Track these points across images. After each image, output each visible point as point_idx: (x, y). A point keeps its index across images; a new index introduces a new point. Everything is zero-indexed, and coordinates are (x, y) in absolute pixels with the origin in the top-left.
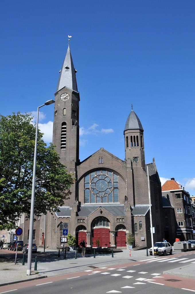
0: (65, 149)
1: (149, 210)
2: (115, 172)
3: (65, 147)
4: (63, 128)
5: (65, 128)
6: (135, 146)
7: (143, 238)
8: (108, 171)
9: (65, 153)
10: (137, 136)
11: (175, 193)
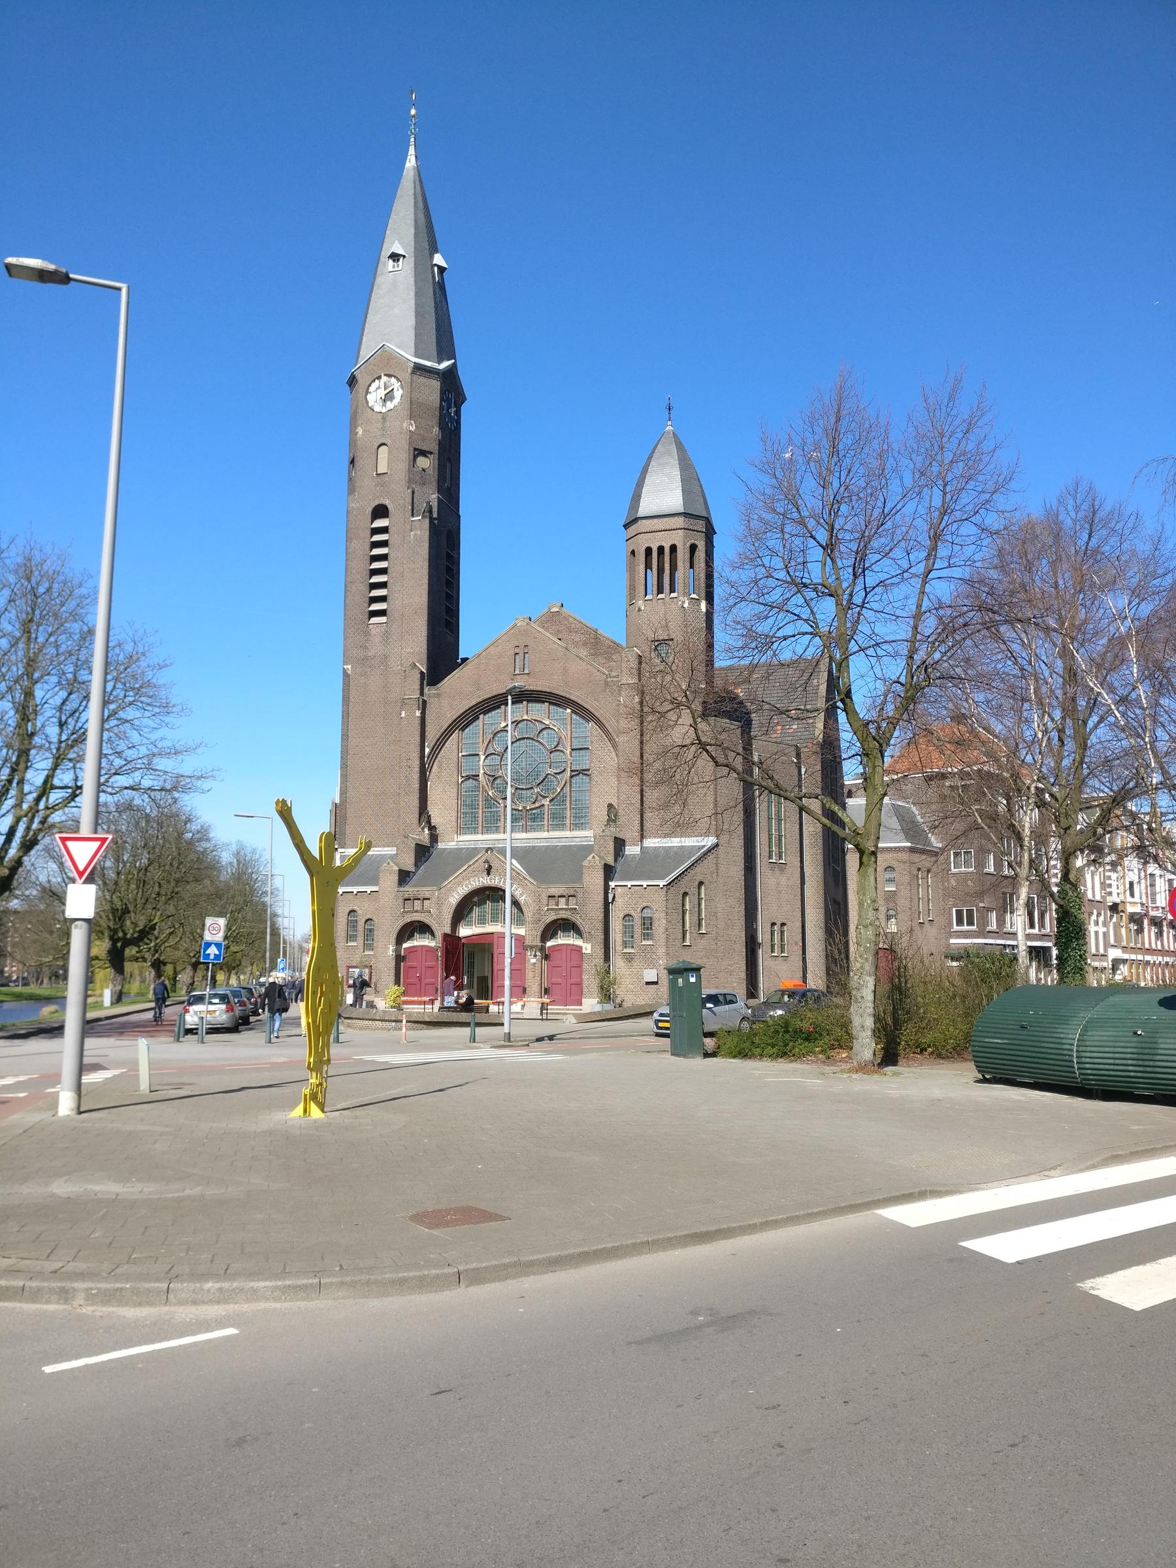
0: (383, 619)
3: (382, 613)
4: (376, 531)
5: (384, 530)
6: (660, 590)
7: (650, 975)
8: (551, 703)
9: (386, 635)
10: (673, 548)
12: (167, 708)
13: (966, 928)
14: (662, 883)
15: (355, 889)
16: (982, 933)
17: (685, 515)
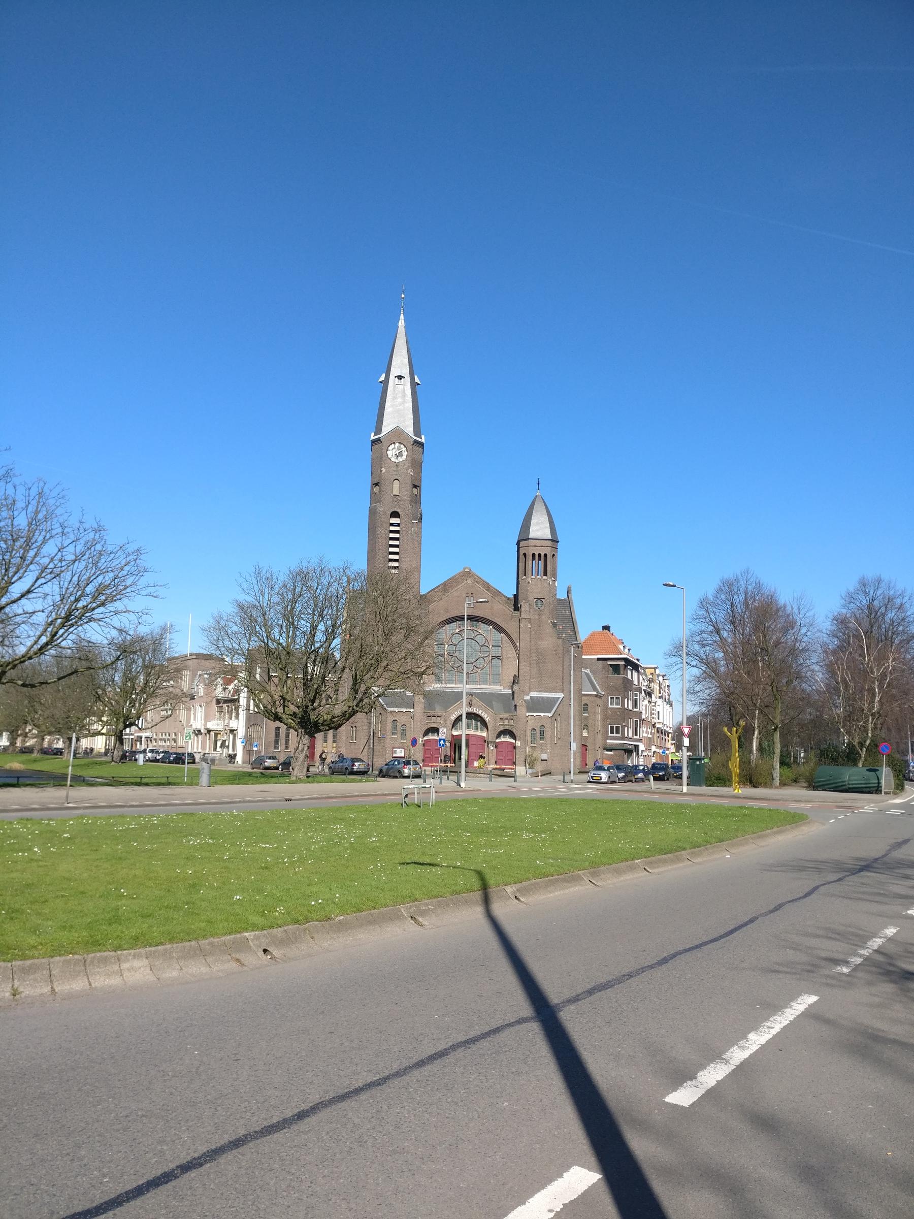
0: (396, 571)
1: (796, 819)
2: (499, 628)
10: (545, 555)
11: (610, 663)
12: (241, 607)
13: (615, 735)
14: (550, 715)
15: (404, 710)
16: (623, 738)
17: (552, 540)
